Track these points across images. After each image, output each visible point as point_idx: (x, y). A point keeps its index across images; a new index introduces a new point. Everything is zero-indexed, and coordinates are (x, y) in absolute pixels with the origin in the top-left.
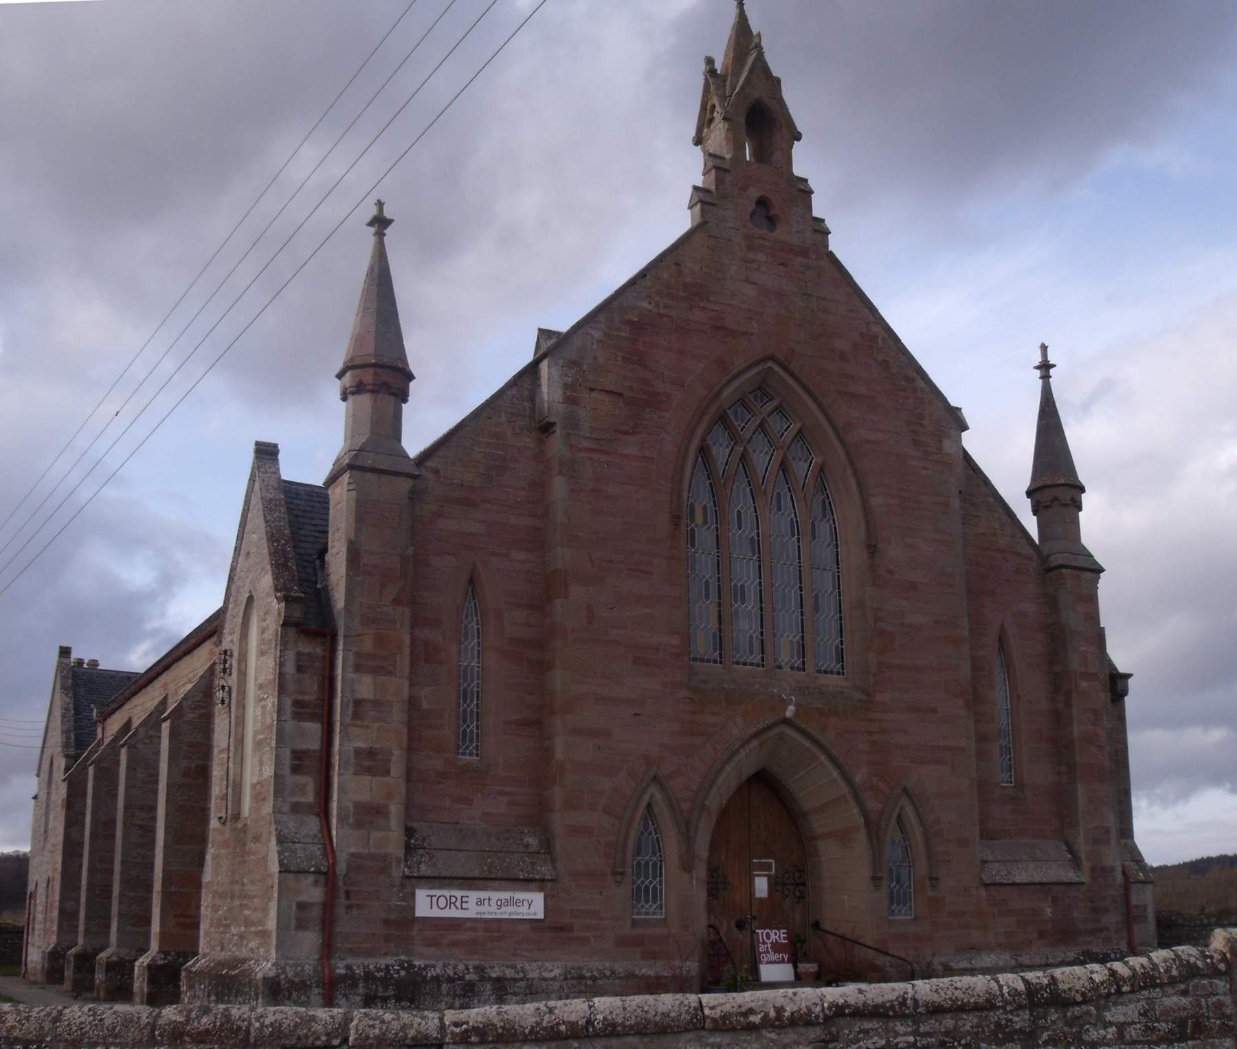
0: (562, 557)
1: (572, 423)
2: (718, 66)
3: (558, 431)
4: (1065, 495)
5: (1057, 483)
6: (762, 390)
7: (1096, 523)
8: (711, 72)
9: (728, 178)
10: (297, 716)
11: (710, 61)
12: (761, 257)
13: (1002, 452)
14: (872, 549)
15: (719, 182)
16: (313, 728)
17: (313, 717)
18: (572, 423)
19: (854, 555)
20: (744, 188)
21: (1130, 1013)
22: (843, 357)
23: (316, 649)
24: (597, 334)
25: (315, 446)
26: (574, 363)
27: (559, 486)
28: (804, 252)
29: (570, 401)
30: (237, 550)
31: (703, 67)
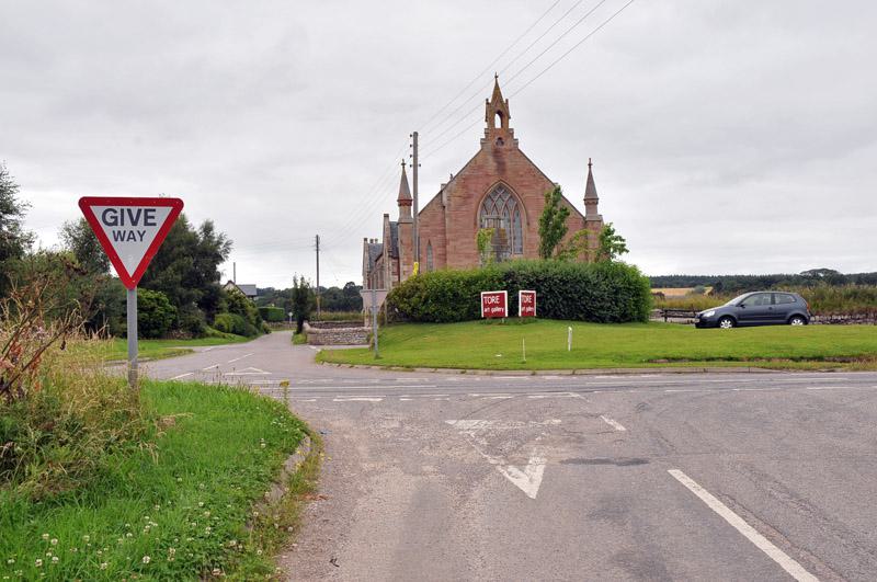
1: (449, 205)
2: (490, 101)
5: (591, 200)
6: (500, 188)
8: (488, 103)
13: (575, 196)
14: (528, 224)
18: (449, 205)
19: (524, 225)
21: (528, 299)
25: (395, 217)
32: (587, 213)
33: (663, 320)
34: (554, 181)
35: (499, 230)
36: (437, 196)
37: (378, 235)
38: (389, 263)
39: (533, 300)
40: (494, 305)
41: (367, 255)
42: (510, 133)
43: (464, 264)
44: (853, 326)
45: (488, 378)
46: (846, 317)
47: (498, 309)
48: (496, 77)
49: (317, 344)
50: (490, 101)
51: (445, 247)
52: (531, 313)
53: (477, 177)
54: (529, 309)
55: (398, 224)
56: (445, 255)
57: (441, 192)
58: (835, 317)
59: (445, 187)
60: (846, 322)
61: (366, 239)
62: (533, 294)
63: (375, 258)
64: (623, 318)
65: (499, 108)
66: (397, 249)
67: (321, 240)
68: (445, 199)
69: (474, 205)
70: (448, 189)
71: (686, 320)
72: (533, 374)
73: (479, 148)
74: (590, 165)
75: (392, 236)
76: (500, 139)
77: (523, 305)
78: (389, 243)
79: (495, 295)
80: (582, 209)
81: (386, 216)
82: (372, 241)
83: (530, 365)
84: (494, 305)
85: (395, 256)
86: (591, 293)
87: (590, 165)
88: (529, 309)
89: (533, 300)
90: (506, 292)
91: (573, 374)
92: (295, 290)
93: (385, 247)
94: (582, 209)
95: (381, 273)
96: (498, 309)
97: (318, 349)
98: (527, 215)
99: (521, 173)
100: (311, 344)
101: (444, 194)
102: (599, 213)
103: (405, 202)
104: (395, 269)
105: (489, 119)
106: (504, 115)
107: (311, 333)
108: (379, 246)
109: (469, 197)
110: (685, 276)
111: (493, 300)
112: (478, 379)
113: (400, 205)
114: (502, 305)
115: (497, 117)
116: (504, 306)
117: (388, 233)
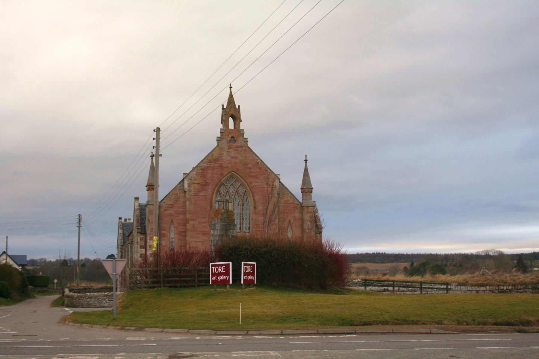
0: (188, 216)
1: (190, 191)
2: (225, 107)
3: (187, 193)
4: (310, 190)
5: (307, 189)
6: (232, 177)
7: (315, 195)
8: (223, 108)
9: (224, 134)
10: (141, 248)
11: (223, 106)
12: (231, 150)
13: (293, 184)
14: (255, 208)
15: (222, 135)
16: (144, 250)
17: (143, 248)
18: (190, 191)
19: (252, 209)
20: (228, 135)
21: (249, 269)
22: (250, 168)
23: (143, 236)
24: (195, 173)
25: (143, 200)
26: (190, 179)
27: (188, 203)
28: (242, 147)
29: (189, 186)
30: (202, 161)
31: (221, 107)
32: (303, 199)
33: (362, 288)
34: (191, 169)
35: (227, 211)
36: (181, 182)
37: (129, 215)
38: (138, 238)
39: (253, 270)
40: (220, 274)
41: (121, 231)
42: (242, 133)
43: (203, 239)
44: (516, 294)
45: (207, 337)
46: (510, 287)
47: (223, 278)
48: (231, 87)
49: (71, 305)
50: (225, 107)
51: (185, 225)
52: (252, 281)
53: (213, 168)
54: (250, 278)
55: (146, 205)
56: (185, 232)
57: (184, 179)
58: (502, 288)
59: (186, 175)
60: (510, 291)
61: (120, 218)
62: (253, 265)
63: (127, 233)
64: (322, 287)
65: (232, 113)
66: (145, 227)
67: (83, 217)
68: (186, 186)
69: (210, 191)
70: (189, 177)
71: (383, 288)
72: (247, 334)
73: (215, 144)
74: (306, 160)
75: (141, 216)
76: (232, 137)
77: (245, 274)
78: (138, 222)
79: (221, 265)
80: (299, 195)
81: (137, 199)
82: (126, 220)
83: (252, 324)
84: (220, 274)
85: (143, 231)
86: (297, 265)
87: (306, 160)
88: (250, 278)
89: (253, 270)
90: (230, 263)
91: (282, 334)
92: (499, 255)
93: (135, 224)
94: (299, 195)
95: (131, 247)
96: (223, 278)
97: (70, 310)
98: (254, 199)
99: (250, 166)
100: (67, 306)
101: (186, 182)
102: (313, 200)
103: (151, 187)
104: (143, 243)
105: (224, 121)
106: (237, 118)
107: (68, 297)
108: (130, 223)
109: (206, 184)
110: (385, 254)
111: (219, 270)
112: (198, 338)
113: (148, 190)
114: (227, 274)
115: (231, 120)
116: (229, 275)
117: (138, 212)
